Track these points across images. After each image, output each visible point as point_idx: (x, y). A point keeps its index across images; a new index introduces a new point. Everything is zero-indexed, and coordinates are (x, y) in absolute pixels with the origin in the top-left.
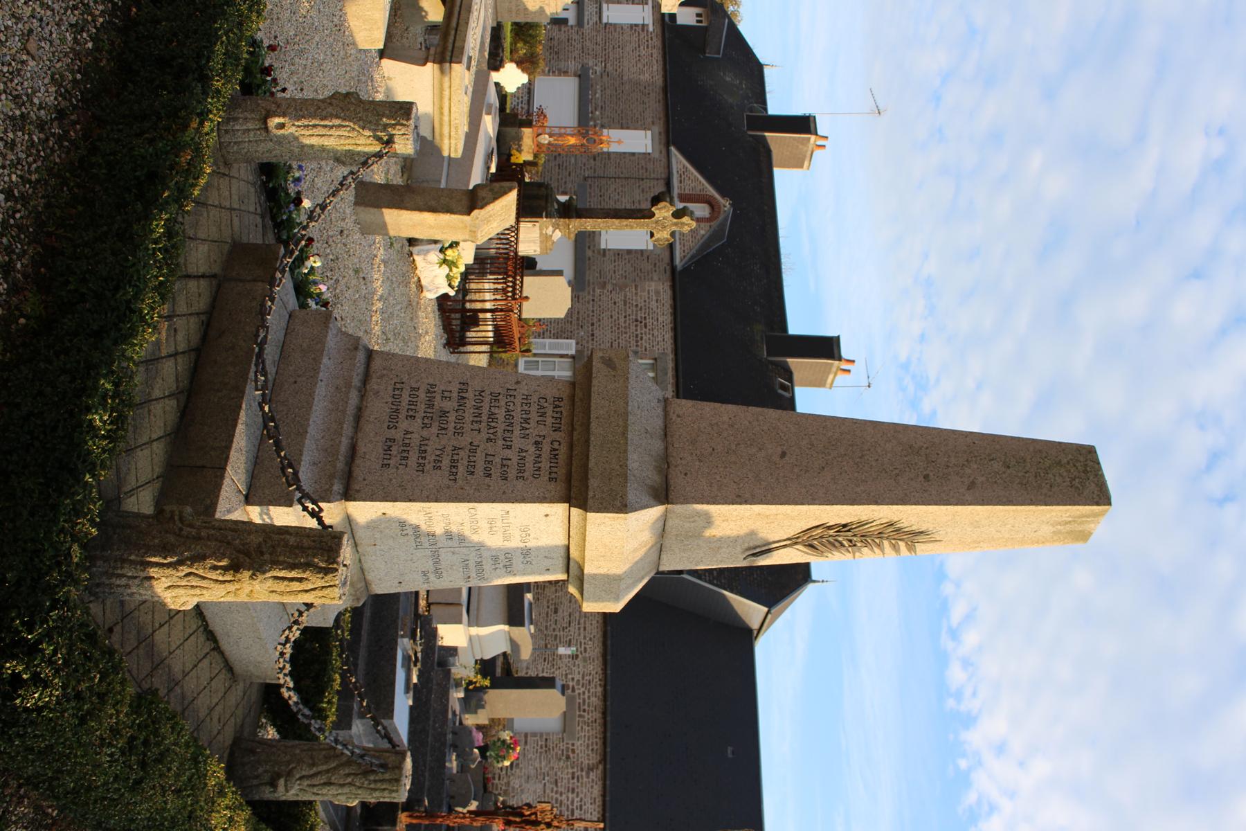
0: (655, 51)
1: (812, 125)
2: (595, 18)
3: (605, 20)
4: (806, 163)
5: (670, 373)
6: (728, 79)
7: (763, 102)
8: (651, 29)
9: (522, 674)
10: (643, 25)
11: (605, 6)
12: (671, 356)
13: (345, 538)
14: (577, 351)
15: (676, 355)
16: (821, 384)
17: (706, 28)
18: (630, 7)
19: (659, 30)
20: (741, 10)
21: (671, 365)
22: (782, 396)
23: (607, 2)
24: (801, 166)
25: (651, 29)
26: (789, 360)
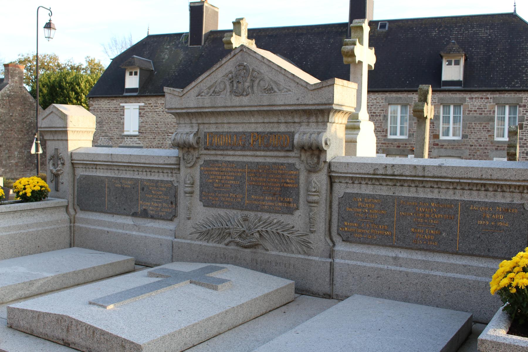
0: (159, 102)
1: (197, 4)
2: (136, 139)
3: (137, 133)
4: (216, 10)
5: (400, 95)
6: (166, 57)
7: (179, 35)
8: (143, 104)
9: (62, 209)
10: (140, 109)
11: (126, 133)
12: (388, 95)
13: (11, 306)
14: (383, 153)
15: (386, 91)
16: (216, 14)
17: (141, 69)
18: (126, 117)
19: (144, 99)
20: (49, 54)
21: (394, 95)
22: (389, 27)
23: (123, 132)
24: (217, 13)
25: (143, 104)
26: (204, 33)
